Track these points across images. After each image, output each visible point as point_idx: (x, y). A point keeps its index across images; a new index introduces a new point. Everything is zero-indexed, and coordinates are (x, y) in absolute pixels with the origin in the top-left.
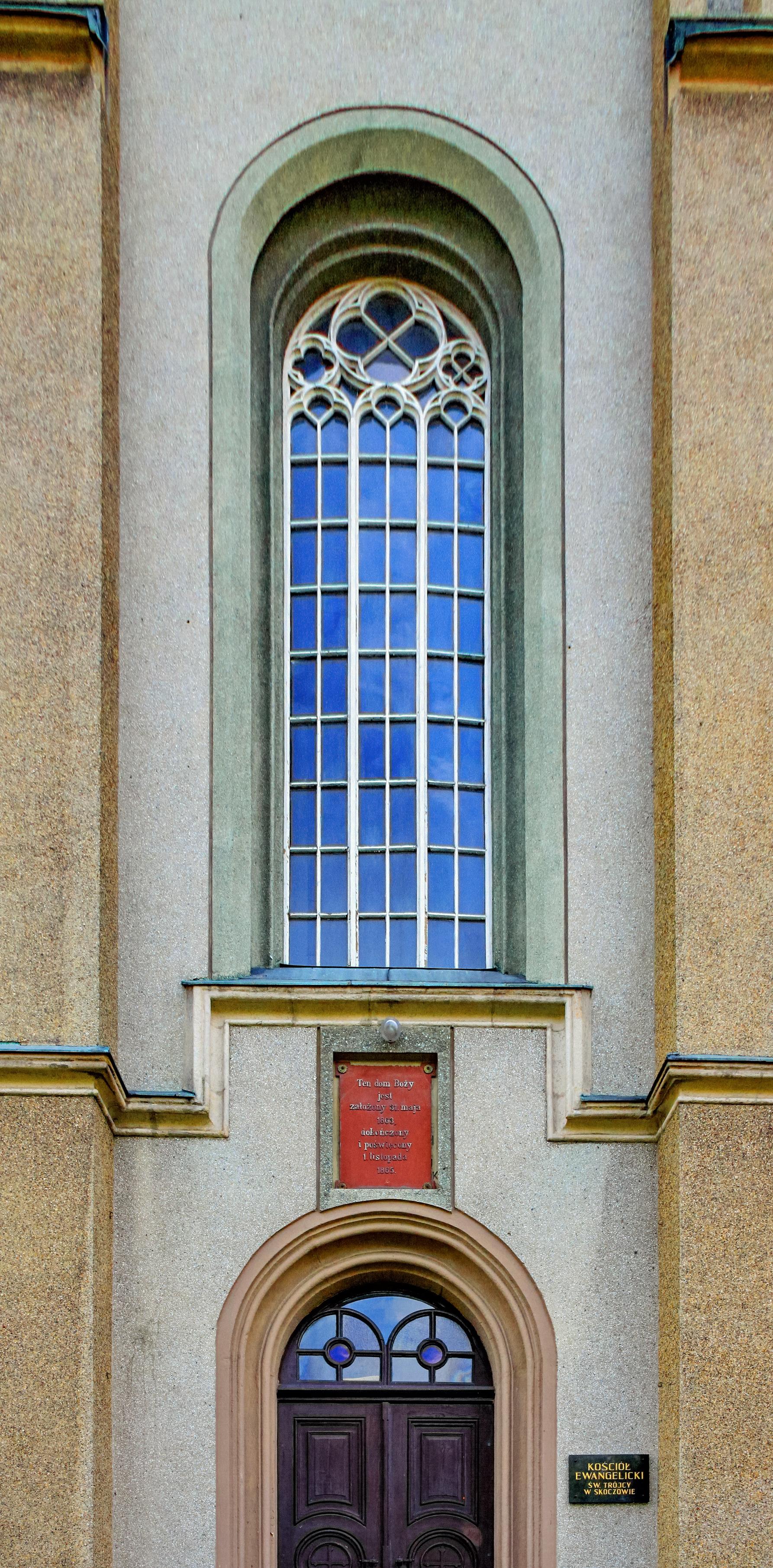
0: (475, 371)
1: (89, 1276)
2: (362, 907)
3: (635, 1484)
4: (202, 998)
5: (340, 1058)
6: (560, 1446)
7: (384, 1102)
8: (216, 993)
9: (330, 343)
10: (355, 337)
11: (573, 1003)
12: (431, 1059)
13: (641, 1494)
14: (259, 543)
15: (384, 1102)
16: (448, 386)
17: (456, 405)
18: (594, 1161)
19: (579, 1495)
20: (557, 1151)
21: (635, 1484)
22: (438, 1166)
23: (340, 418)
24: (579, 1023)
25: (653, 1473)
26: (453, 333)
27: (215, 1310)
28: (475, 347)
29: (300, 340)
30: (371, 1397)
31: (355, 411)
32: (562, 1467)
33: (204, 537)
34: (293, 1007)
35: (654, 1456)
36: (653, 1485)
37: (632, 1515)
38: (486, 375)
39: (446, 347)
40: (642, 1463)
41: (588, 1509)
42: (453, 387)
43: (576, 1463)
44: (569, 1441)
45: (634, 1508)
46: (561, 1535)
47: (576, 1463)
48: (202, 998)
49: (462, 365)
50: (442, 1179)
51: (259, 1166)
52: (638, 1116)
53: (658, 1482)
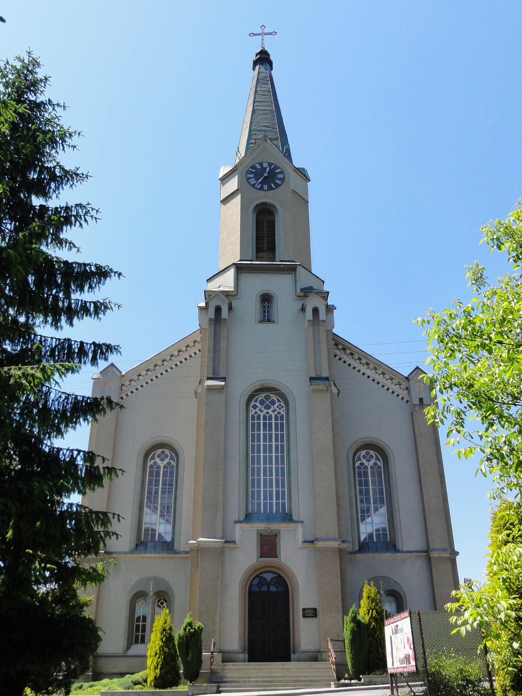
0: (282, 407)
1: (220, 578)
3: (314, 614)
7: (268, 545)
9: (258, 404)
10: (262, 402)
12: (225, 378)
13: (315, 615)
15: (268, 545)
16: (278, 410)
17: (279, 413)
19: (304, 616)
21: (314, 614)
23: (259, 415)
26: (279, 401)
28: (282, 404)
29: (252, 404)
30: (260, 496)
35: (318, 608)
36: (318, 614)
37: (314, 619)
38: (284, 408)
39: (277, 404)
40: (315, 610)
41: (306, 618)
43: (304, 610)
45: (314, 618)
47: (304, 610)
50: (278, 556)
51: (245, 558)
53: (194, 340)
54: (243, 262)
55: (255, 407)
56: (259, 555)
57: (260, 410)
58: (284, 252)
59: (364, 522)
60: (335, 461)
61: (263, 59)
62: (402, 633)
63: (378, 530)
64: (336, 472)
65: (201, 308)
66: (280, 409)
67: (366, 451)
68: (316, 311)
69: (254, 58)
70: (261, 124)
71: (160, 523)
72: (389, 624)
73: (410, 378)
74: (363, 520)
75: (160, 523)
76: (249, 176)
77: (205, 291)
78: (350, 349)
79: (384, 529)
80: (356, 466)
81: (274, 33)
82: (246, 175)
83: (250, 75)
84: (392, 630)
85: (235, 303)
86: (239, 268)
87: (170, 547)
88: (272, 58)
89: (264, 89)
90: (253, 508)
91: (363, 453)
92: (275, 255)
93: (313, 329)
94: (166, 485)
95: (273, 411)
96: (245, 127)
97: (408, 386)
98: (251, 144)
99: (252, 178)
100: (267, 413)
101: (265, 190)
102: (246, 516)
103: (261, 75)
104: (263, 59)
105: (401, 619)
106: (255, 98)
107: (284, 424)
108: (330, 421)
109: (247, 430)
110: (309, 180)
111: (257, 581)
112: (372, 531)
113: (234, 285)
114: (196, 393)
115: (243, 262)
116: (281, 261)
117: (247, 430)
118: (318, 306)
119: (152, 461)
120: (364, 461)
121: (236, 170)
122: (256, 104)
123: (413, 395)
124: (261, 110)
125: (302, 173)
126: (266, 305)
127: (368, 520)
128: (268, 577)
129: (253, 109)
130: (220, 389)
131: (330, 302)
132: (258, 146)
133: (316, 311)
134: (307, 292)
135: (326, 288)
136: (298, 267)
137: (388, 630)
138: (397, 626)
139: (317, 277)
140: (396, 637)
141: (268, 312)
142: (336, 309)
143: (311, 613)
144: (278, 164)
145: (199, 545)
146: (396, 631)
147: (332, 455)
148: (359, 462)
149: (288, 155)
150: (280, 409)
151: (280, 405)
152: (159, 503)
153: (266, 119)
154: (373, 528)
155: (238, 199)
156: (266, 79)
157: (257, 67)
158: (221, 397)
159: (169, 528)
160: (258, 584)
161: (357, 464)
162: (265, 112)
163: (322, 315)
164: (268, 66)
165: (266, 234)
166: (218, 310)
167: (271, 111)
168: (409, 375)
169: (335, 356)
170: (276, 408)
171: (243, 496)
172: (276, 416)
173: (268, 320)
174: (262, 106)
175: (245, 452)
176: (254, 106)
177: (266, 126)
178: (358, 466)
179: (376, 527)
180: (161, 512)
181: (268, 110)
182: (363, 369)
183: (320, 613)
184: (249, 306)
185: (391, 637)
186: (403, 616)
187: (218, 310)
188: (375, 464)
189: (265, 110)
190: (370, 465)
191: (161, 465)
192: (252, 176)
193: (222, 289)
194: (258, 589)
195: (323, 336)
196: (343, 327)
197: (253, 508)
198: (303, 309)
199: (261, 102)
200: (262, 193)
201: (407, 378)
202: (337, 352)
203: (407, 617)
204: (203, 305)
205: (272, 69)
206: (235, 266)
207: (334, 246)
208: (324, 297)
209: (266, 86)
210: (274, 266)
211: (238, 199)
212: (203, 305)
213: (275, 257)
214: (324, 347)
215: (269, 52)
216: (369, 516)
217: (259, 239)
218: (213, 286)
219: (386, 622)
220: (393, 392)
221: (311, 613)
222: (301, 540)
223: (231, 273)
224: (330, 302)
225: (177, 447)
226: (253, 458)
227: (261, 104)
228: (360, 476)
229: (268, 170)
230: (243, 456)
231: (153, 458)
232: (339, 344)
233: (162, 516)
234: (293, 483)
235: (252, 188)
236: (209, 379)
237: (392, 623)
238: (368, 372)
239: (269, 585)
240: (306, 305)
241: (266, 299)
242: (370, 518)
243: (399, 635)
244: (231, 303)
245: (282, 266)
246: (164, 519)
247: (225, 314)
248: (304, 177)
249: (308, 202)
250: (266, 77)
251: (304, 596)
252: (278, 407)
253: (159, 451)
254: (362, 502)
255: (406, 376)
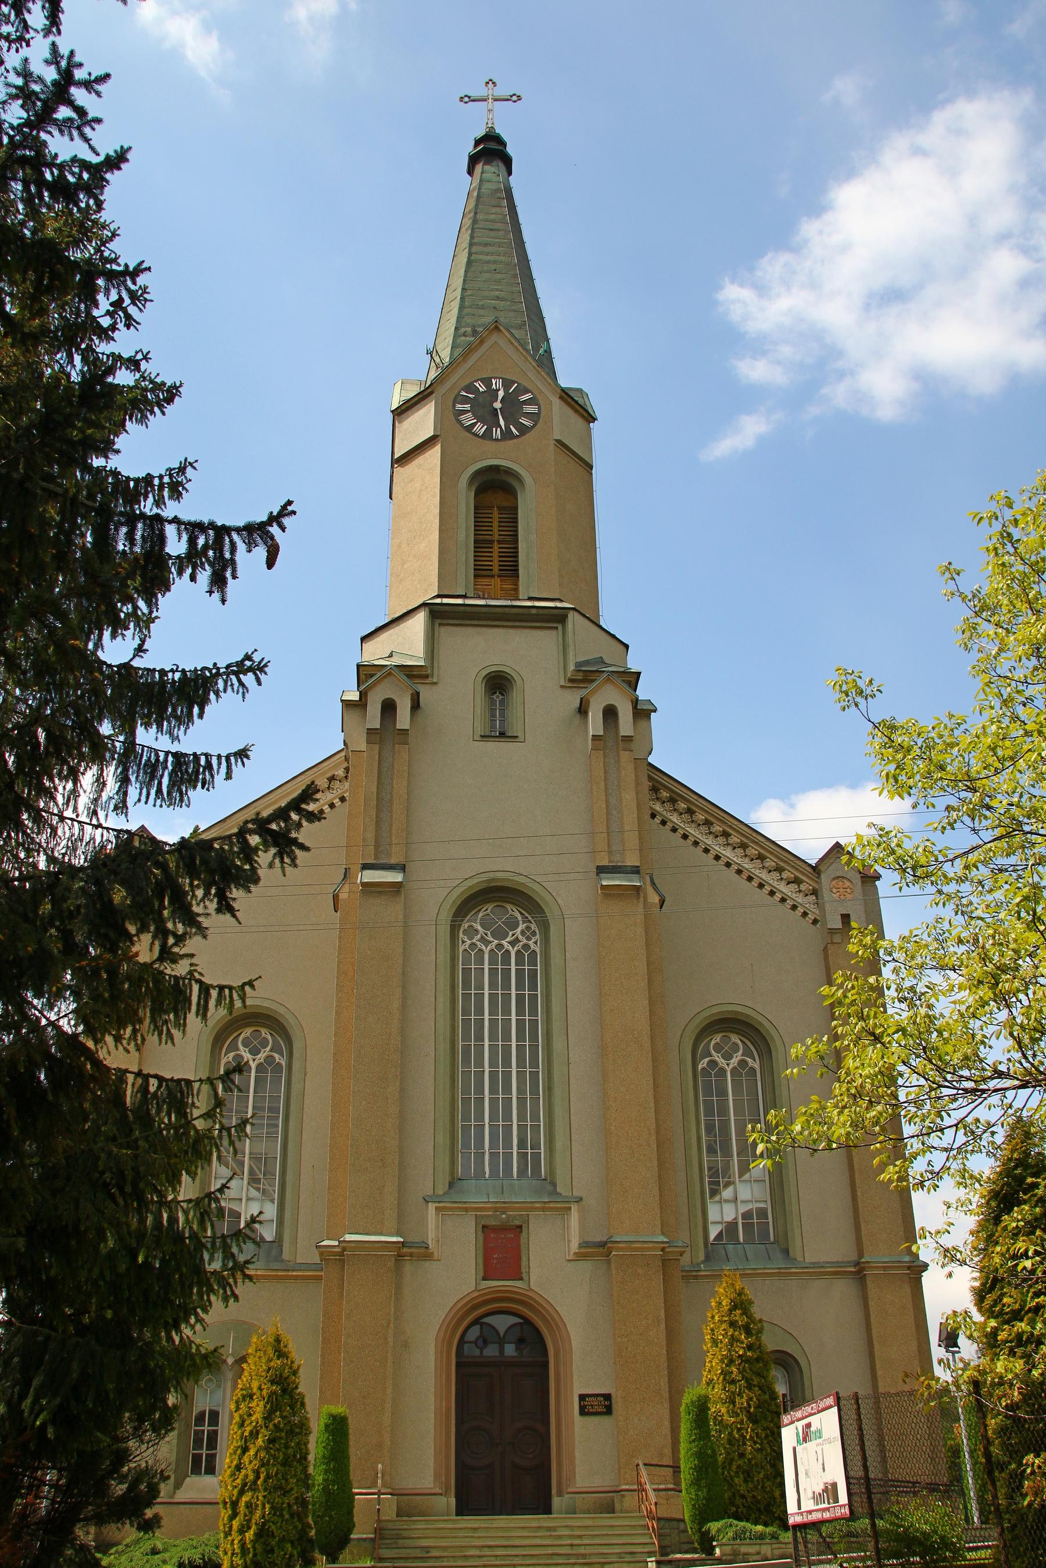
0: (534, 933)
1: (392, 1325)
2: (490, 1121)
3: (606, 1406)
4: (432, 1207)
5: (483, 1227)
6: (575, 1389)
7: (502, 1246)
8: (437, 1205)
11: (574, 1207)
13: (609, 1411)
14: (413, 614)
15: (502, 1246)
17: (526, 947)
18: (586, 1266)
19: (583, 1412)
20: (569, 1264)
21: (606, 1406)
22: (523, 1270)
24: (576, 1214)
25: (613, 1401)
27: (435, 1332)
28: (533, 926)
31: (487, 951)
32: (576, 1399)
33: (433, 1024)
34: (466, 1210)
36: (614, 1406)
37: (605, 1420)
38: (538, 936)
40: (607, 1397)
42: (525, 941)
43: (582, 1397)
44: (578, 1389)
46: (576, 1430)
47: (582, 1397)
48: (432, 1207)
49: (528, 933)
50: (524, 1276)
51: (454, 1277)
52: (598, 1250)
54: (446, 601)
55: (471, 932)
56: (481, 1274)
57: (483, 940)
58: (535, 587)
59: (717, 1198)
60: (654, 1059)
61: (491, 150)
62: (819, 1441)
63: (747, 1215)
64: (656, 1086)
65: (347, 704)
66: (528, 939)
67: (721, 1035)
68: (610, 713)
69: (469, 148)
70: (486, 293)
71: (248, 1199)
72: (792, 1422)
73: (822, 868)
74: (714, 1193)
75: (248, 1199)
76: (459, 407)
77: (358, 666)
78: (688, 801)
79: (762, 1213)
80: (700, 1067)
81: (514, 98)
82: (454, 406)
83: (454, 188)
84: (797, 1434)
85: (426, 694)
86: (438, 615)
87: (274, 1252)
88: (510, 150)
89: (493, 217)
90: (466, 1166)
91: (717, 1038)
92: (516, 584)
93: (605, 756)
94: (263, 1109)
95: (513, 943)
96: (450, 297)
97: (816, 886)
98: (465, 335)
99: (467, 411)
100: (500, 946)
101: (497, 440)
102: (451, 1185)
103: (486, 186)
104: (491, 150)
105: (819, 1412)
106: (472, 237)
107: (534, 975)
108: (643, 968)
109: (453, 987)
110: (594, 419)
111: (474, 1333)
112: (735, 1219)
113: (426, 652)
114: (336, 897)
115: (446, 601)
116: (530, 599)
117: (453, 987)
118: (617, 705)
119: (231, 1055)
120: (717, 1057)
121: (431, 393)
122: (474, 249)
123: (827, 906)
124: (488, 262)
125: (577, 405)
126: (497, 697)
127: (727, 1193)
128: (502, 1323)
129: (469, 259)
130: (396, 888)
131: (642, 693)
132: (482, 342)
133: (610, 713)
134: (585, 676)
135: (633, 665)
136: (571, 614)
137: (789, 1435)
138: (809, 1425)
139: (613, 636)
140: (806, 1448)
141: (502, 715)
142: (655, 711)
143: (597, 1406)
144: (525, 383)
145: (344, 1249)
146: (806, 1436)
147: (647, 1045)
148: (706, 1060)
149: (546, 363)
150: (528, 939)
151: (528, 928)
152: (247, 1151)
153: (499, 282)
154: (737, 1211)
155: (434, 456)
156: (499, 195)
157: (479, 168)
158: (392, 910)
159: (270, 1211)
160: (477, 1339)
161: (703, 1064)
162: (493, 267)
163: (626, 724)
164: (502, 168)
165: (496, 537)
166: (389, 708)
167: (508, 264)
168: (822, 860)
169: (653, 816)
170: (520, 937)
171: (443, 1139)
172: (518, 952)
173: (502, 734)
174: (487, 254)
175: (448, 1110)
176: (470, 254)
177: (498, 298)
178: (704, 1068)
179: (743, 1209)
180: (252, 1172)
181: (501, 262)
182: (717, 846)
183: (617, 1405)
184: (457, 700)
185: (794, 1449)
186: (822, 1405)
187: (389, 708)
188: (743, 1063)
189: (495, 262)
190: (731, 1066)
191: (484, 948)
192: (467, 407)
193: (396, 661)
194: (477, 1352)
195: (628, 772)
196: (671, 753)
197: (466, 1166)
198: (582, 710)
199: (486, 245)
200: (489, 445)
201: (816, 869)
202: (658, 807)
203: (830, 1407)
204: (354, 696)
205: (510, 173)
206: (427, 609)
207: (647, 579)
208: (629, 683)
209: (498, 210)
210: (514, 611)
211: (434, 456)
212: (354, 696)
213: (516, 590)
214: (629, 797)
215: (505, 137)
216: (727, 1185)
217: (481, 544)
218: (376, 652)
219: (785, 1419)
220: (783, 900)
221: (597, 1406)
222: (574, 1246)
223: (419, 622)
224: (642, 693)
225: (290, 1023)
226: (467, 1049)
227: (486, 249)
228: (708, 1092)
229: (501, 394)
230: (444, 1046)
231: (233, 1047)
232: (662, 788)
233: (254, 1180)
234: (558, 1111)
235: (467, 434)
236: (366, 867)
237: (799, 1420)
238: (728, 853)
239: (501, 1342)
240: (588, 702)
241: (498, 684)
242: (731, 1189)
243: (811, 1445)
244: (418, 694)
245: (534, 611)
246: (258, 1189)
247: (403, 718)
248: (582, 411)
249: (591, 467)
250: (498, 190)
251: (583, 1364)
252: (523, 933)
253: (247, 1032)
254: (711, 1150)
255: (813, 862)
